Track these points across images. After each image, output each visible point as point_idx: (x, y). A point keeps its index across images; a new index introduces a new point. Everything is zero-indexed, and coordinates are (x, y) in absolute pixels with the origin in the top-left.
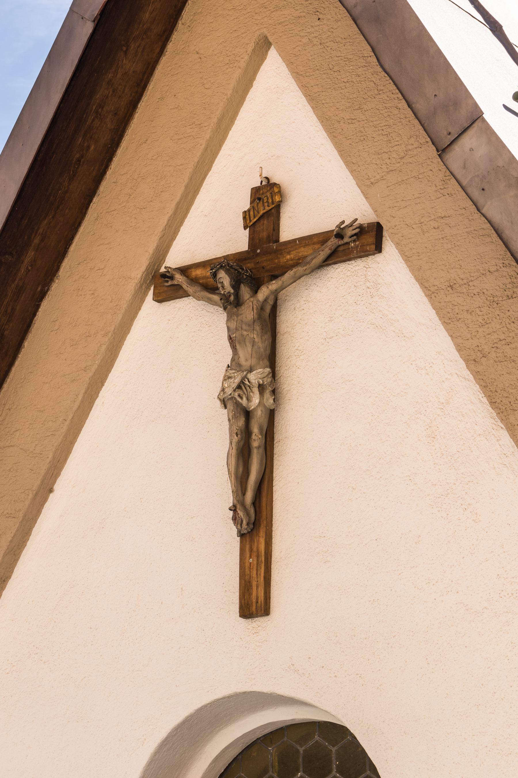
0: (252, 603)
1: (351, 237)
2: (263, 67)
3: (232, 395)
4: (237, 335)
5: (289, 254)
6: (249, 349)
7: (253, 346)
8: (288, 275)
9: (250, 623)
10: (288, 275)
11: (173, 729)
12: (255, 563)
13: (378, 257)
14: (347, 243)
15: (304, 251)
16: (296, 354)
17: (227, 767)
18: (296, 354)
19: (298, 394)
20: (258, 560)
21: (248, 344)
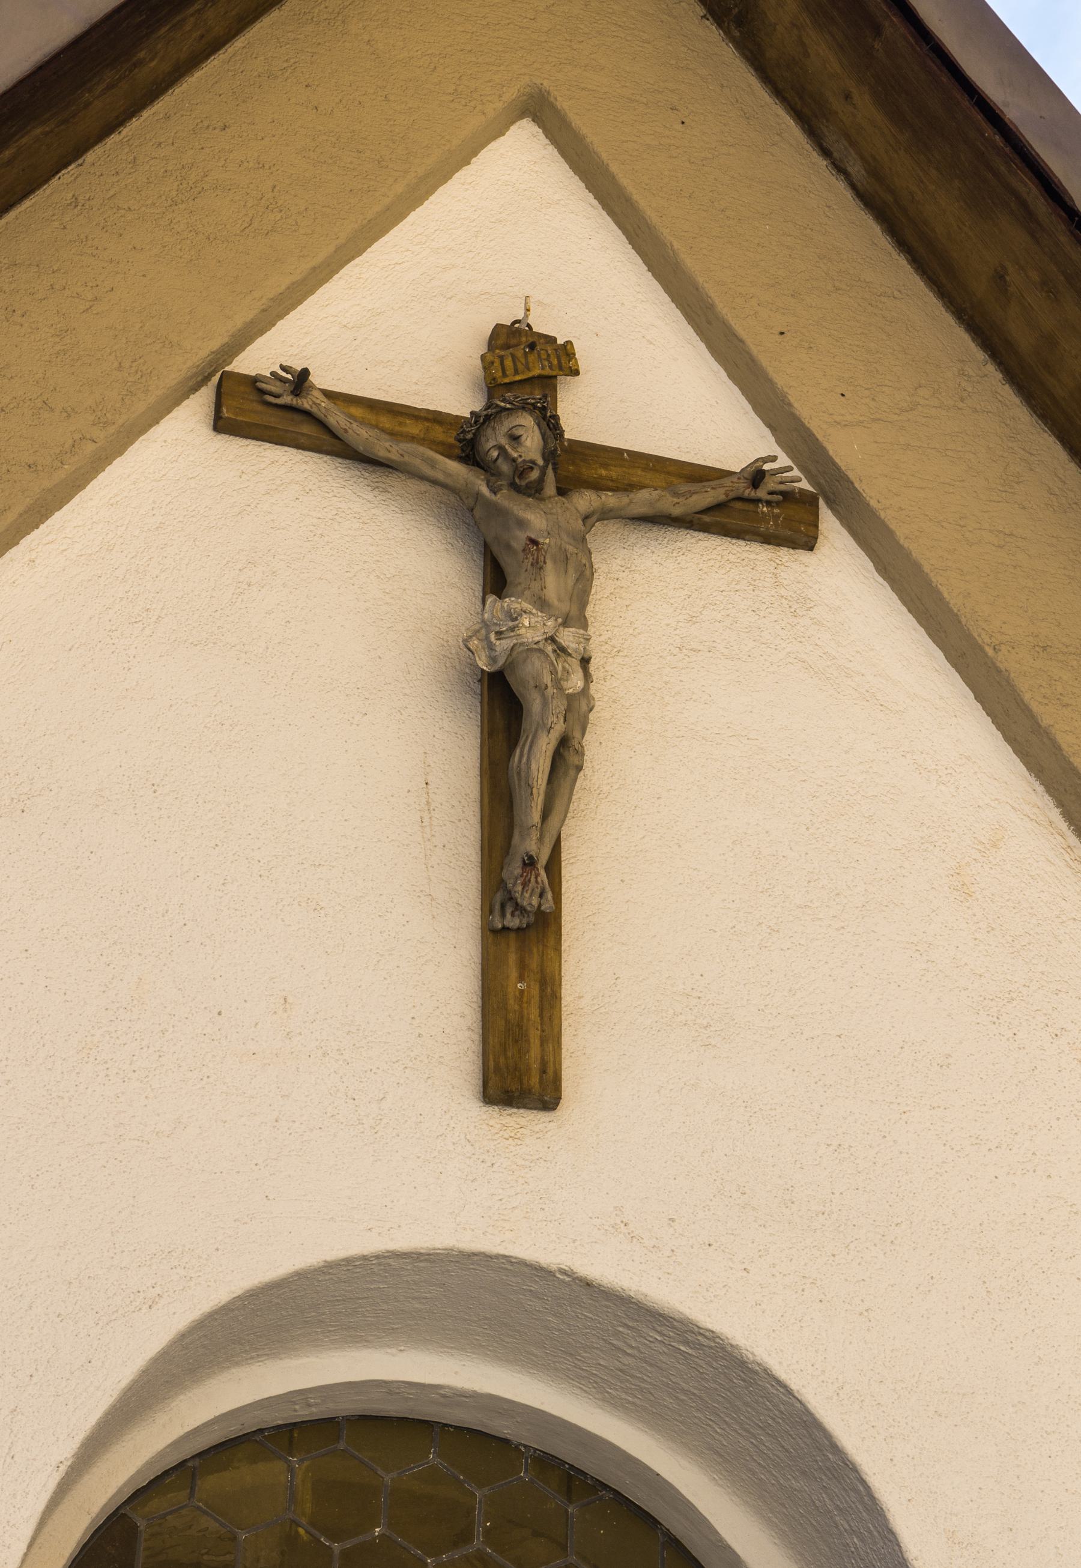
0: (529, 1069)
1: (771, 493)
2: (493, 145)
3: (541, 645)
4: (552, 543)
5: (606, 469)
6: (571, 582)
7: (577, 580)
8: (647, 495)
9: (495, 1114)
10: (647, 495)
11: (248, 1291)
12: (535, 991)
13: (802, 555)
14: (757, 501)
15: (638, 475)
16: (603, 649)
17: (158, 1478)
18: (603, 649)
19: (613, 721)
20: (542, 990)
21: (571, 570)
